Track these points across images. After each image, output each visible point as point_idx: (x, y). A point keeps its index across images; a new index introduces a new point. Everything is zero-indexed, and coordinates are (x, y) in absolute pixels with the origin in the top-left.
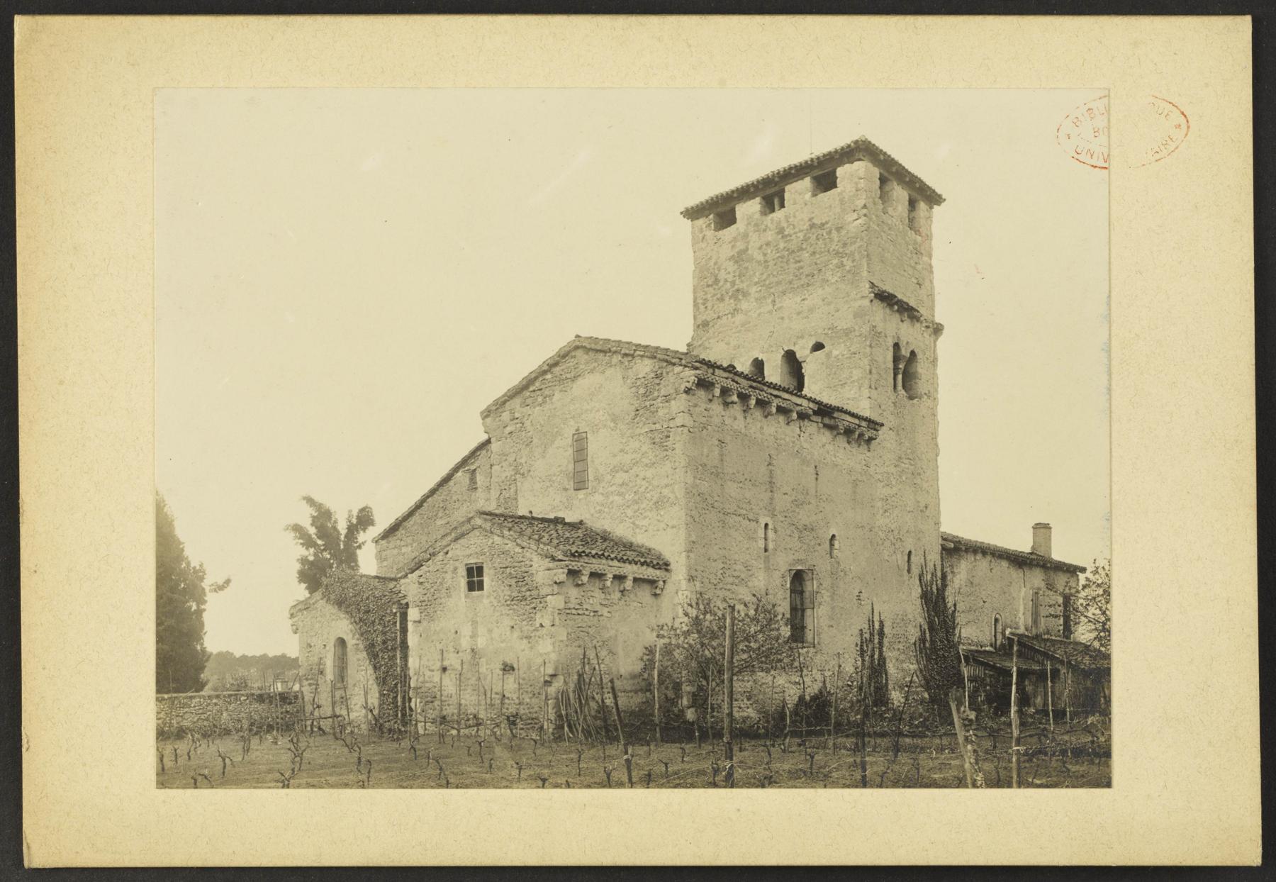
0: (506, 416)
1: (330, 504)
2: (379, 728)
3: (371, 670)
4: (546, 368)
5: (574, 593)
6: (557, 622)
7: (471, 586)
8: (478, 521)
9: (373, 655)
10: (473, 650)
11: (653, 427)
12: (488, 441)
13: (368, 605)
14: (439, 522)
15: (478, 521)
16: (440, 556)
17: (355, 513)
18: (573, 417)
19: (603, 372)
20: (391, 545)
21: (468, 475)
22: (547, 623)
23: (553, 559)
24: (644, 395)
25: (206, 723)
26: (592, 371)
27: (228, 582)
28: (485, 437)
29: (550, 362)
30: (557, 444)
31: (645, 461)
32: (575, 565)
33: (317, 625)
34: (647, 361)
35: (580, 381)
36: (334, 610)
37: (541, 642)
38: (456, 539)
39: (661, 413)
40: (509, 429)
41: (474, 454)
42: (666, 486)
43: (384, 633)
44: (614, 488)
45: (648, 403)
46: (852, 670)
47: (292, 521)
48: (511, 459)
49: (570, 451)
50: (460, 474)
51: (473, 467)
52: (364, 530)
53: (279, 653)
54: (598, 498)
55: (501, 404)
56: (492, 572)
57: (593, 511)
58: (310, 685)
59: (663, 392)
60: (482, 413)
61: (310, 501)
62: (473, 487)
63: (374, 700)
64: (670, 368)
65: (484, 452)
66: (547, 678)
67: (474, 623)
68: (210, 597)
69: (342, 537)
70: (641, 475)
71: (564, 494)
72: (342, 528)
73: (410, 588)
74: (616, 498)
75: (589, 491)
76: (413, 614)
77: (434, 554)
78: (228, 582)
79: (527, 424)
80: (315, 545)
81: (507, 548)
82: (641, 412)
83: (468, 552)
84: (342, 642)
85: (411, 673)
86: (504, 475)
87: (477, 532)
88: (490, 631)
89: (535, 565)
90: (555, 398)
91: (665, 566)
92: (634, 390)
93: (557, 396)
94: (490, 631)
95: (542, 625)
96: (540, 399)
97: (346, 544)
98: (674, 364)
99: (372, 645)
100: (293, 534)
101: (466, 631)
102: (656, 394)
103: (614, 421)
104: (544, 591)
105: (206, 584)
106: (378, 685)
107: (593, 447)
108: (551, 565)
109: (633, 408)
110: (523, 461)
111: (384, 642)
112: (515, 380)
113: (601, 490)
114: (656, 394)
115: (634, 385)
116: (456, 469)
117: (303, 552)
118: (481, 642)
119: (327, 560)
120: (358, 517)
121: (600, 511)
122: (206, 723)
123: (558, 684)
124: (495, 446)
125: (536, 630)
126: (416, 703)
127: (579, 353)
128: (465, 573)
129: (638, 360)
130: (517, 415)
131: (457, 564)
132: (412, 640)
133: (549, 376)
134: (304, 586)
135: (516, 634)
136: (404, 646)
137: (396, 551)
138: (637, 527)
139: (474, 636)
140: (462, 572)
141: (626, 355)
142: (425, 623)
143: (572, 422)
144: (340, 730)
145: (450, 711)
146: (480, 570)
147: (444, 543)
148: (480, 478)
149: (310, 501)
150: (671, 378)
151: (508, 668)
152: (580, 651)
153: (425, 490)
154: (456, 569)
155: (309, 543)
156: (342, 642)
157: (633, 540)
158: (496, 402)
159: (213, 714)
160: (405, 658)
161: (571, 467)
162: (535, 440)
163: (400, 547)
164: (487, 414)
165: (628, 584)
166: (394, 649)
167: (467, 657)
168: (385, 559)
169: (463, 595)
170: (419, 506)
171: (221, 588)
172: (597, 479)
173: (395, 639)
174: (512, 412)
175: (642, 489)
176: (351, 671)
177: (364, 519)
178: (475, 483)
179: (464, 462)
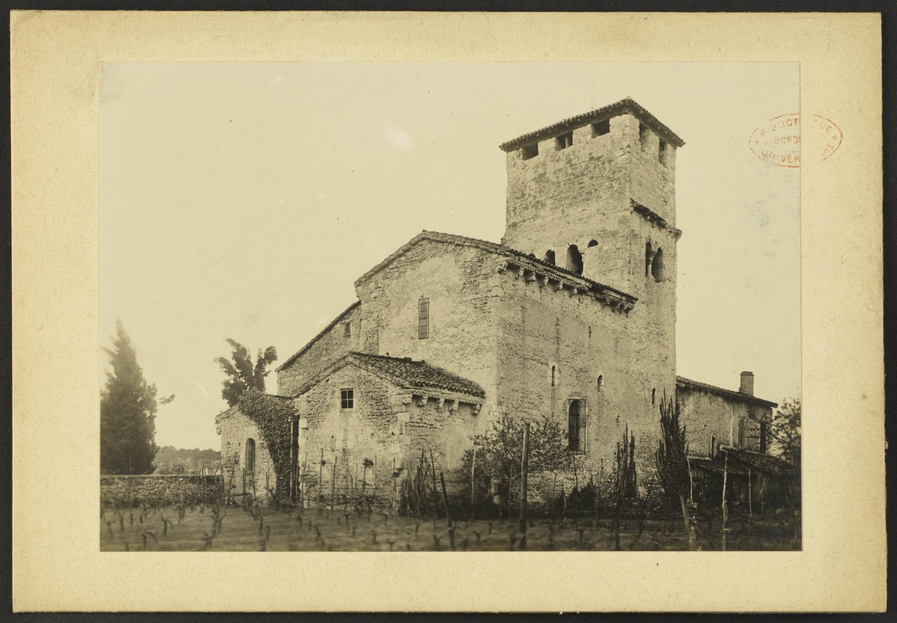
0: (372, 285)
3: (271, 462)
4: (401, 252)
8: (350, 359)
9: (272, 447)
12: (359, 303)
15: (350, 359)
16: (323, 383)
17: (263, 351)
18: (419, 288)
20: (288, 374)
23: (403, 387)
25: (154, 497)
27: (173, 397)
28: (357, 300)
29: (405, 248)
31: (470, 320)
32: (419, 392)
34: (473, 250)
35: (425, 263)
37: (392, 445)
38: (335, 371)
39: (481, 286)
40: (374, 295)
41: (348, 312)
42: (484, 338)
43: (282, 436)
44: (447, 338)
50: (338, 325)
51: (348, 321)
52: (270, 363)
54: (435, 345)
55: (368, 277)
56: (359, 395)
58: (228, 471)
59: (483, 272)
60: (355, 283)
61: (232, 342)
62: (347, 335)
63: (273, 483)
64: (488, 255)
66: (396, 471)
68: (160, 407)
69: (254, 368)
70: (466, 330)
71: (412, 341)
72: (254, 362)
73: (301, 405)
75: (429, 340)
76: (303, 423)
77: (318, 381)
78: (173, 397)
79: (387, 291)
80: (234, 373)
81: (370, 378)
84: (251, 442)
85: (300, 464)
87: (349, 367)
88: (356, 437)
89: (390, 391)
90: (407, 274)
91: (481, 394)
92: (463, 269)
93: (409, 272)
94: (356, 437)
95: (393, 434)
96: (397, 274)
97: (256, 372)
98: (492, 253)
100: (219, 364)
104: (395, 410)
105: (157, 398)
106: (276, 472)
107: (433, 309)
108: (401, 391)
109: (462, 282)
110: (383, 317)
111: (282, 442)
113: (438, 340)
115: (463, 266)
117: (226, 377)
118: (350, 445)
119: (243, 385)
122: (154, 497)
124: (363, 306)
125: (389, 437)
127: (425, 242)
128: (340, 395)
130: (380, 285)
131: (335, 388)
132: (301, 441)
133: (403, 258)
134: (226, 401)
135: (375, 439)
136: (296, 446)
137: (292, 379)
140: (338, 394)
141: (458, 245)
142: (311, 430)
143: (418, 291)
145: (326, 492)
146: (351, 393)
147: (326, 373)
148: (352, 328)
149: (232, 342)
150: (489, 262)
151: (368, 463)
152: (420, 452)
154: (334, 392)
155: (230, 370)
156: (251, 442)
157: (460, 375)
158: (365, 276)
161: (417, 322)
162: (392, 303)
164: (359, 283)
166: (288, 448)
167: (339, 454)
169: (338, 411)
170: (309, 347)
171: (168, 401)
172: (435, 331)
173: (289, 441)
174: (376, 283)
175: (467, 340)
176: (258, 461)
177: (270, 356)
178: (349, 332)
179: (342, 317)
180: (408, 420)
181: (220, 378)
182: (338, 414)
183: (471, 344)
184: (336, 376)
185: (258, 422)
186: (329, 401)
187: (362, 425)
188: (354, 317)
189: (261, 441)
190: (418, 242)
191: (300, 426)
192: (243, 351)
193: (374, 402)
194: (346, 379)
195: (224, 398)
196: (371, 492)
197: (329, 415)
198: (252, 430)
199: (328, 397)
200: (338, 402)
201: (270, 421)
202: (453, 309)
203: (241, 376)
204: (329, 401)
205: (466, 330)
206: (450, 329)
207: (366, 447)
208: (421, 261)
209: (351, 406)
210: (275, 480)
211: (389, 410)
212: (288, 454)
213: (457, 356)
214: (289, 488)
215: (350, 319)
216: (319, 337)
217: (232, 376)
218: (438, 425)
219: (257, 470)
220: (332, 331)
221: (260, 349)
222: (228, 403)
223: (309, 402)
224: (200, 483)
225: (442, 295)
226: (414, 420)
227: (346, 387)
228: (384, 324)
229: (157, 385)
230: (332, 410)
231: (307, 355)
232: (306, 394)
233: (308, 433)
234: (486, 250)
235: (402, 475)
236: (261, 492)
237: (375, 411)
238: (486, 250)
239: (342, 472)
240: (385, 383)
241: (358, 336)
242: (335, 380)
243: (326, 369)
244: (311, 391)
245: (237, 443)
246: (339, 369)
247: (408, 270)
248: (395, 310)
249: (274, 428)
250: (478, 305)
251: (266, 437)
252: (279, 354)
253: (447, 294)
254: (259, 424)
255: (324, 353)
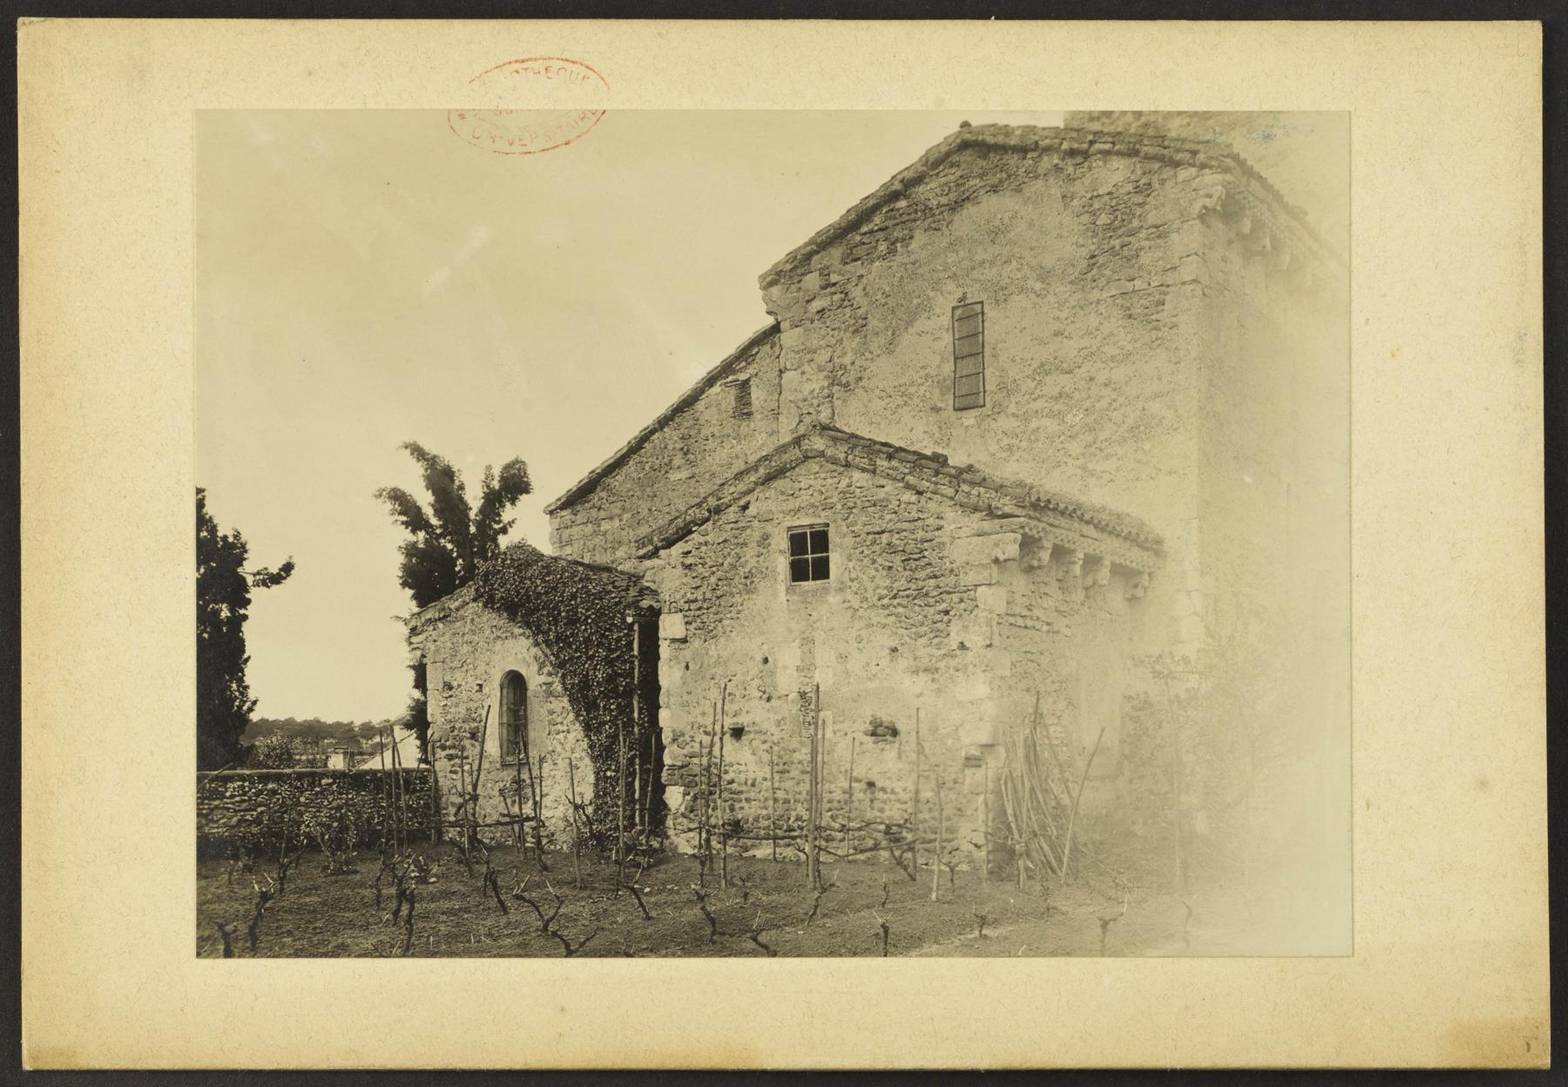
0: (812, 281)
1: (449, 456)
2: (594, 840)
3: (577, 731)
4: (897, 186)
5: (1020, 583)
6: (996, 642)
7: (799, 572)
8: (819, 443)
9: (583, 699)
10: (803, 695)
11: (1129, 286)
12: (776, 329)
13: (574, 610)
14: (674, 476)
15: (819, 443)
16: (731, 514)
17: (497, 472)
18: (954, 277)
19: (1018, 190)
20: (580, 518)
21: (732, 393)
22: (975, 640)
23: (991, 513)
24: (1108, 227)
25: (255, 830)
26: (995, 189)
27: (288, 568)
28: (769, 321)
29: (909, 175)
30: (919, 325)
31: (1111, 350)
32: (1035, 528)
33: (466, 648)
34: (1117, 163)
35: (970, 210)
36: (500, 620)
37: (960, 677)
38: (769, 479)
39: (1146, 259)
40: (817, 305)
41: (746, 353)
42: (1156, 396)
43: (610, 663)
44: (1040, 404)
45: (1116, 243)
46: (1089, 739)
47: (390, 483)
48: (822, 357)
49: (947, 338)
50: (716, 389)
51: (743, 377)
52: (513, 501)
53: (310, 717)
54: (1005, 422)
55: (801, 261)
56: (849, 541)
57: (993, 448)
58: (450, 758)
59: (1152, 218)
60: (762, 277)
61: (418, 452)
62: (743, 410)
63: (587, 791)
64: (1168, 172)
65: (767, 348)
66: (975, 752)
67: (807, 642)
68: (256, 594)
69: (472, 515)
70: (1102, 377)
71: (933, 417)
72: (474, 498)
73: (668, 577)
74: (1046, 422)
75: (987, 410)
76: (671, 626)
77: (718, 510)
78: (288, 568)
79: (856, 293)
80: (426, 526)
81: (882, 494)
82: (1101, 260)
83: (792, 504)
84: (515, 681)
85: (666, 738)
86: (807, 388)
87: (814, 466)
88: (843, 658)
89: (949, 528)
90: (914, 245)
91: (1155, 547)
92: (1086, 218)
93: (920, 238)
94: (843, 658)
95: (962, 646)
96: (883, 247)
97: (479, 525)
98: (1177, 164)
99: (585, 685)
100: (389, 505)
101: (788, 657)
102: (1136, 223)
103: (1042, 279)
104: (968, 579)
105: (248, 568)
106: (594, 759)
107: (997, 325)
108: (987, 525)
109: (1085, 252)
110: (847, 361)
111: (610, 679)
112: (832, 213)
113: (1012, 409)
114: (1136, 223)
115: (1088, 209)
116: (710, 381)
117: (405, 536)
118: (823, 677)
119: (452, 555)
120: (502, 478)
121: (1010, 448)
122: (255, 830)
123: (994, 764)
124: (789, 337)
125: (951, 655)
126: (675, 797)
127: (967, 157)
128: (785, 544)
129: (1097, 162)
130: (834, 278)
131: (769, 528)
132: (669, 675)
133: (903, 204)
134: (409, 592)
135: (903, 663)
136: (651, 688)
137: (589, 528)
138: (1092, 474)
139: (806, 668)
140: (781, 542)
141: (1072, 153)
142: (696, 644)
143: (951, 286)
144: (526, 843)
145: (747, 811)
146: (821, 540)
147: (742, 487)
148: (757, 395)
149: (418, 452)
150: (1171, 191)
151: (884, 732)
152: (1030, 699)
153: (648, 419)
154: (766, 537)
155: (415, 520)
156: (515, 681)
157: (1083, 499)
158: (792, 257)
159: (303, 840)
160: (653, 707)
161: (948, 368)
162: (873, 323)
163: (597, 522)
164: (773, 279)
165: (1104, 574)
166: (628, 694)
167: (791, 708)
168: (570, 543)
169: (782, 588)
170: (636, 448)
171: (276, 579)
172: (1002, 387)
173: (630, 674)
174: (825, 273)
175: (1104, 403)
176: (537, 732)
177: (513, 485)
178: (749, 404)
179: (727, 368)
180: (1002, 609)
181: (391, 542)
182: (783, 597)
183: (1117, 415)
184: (771, 493)
185: (534, 627)
186: (752, 563)
187: (858, 624)
188: (761, 369)
189: (543, 679)
190: (948, 154)
191: (662, 634)
192: (448, 473)
193: (898, 559)
194: (804, 498)
195: (405, 584)
196: (894, 813)
197: (758, 601)
198: (517, 651)
199: (750, 553)
200: (782, 564)
201: (573, 621)
202: (1057, 326)
203: (442, 535)
204: (752, 563)
205: (1102, 377)
206: (1049, 379)
207: (873, 685)
208: (955, 206)
209: (822, 571)
210: (592, 778)
211: (950, 580)
212: (626, 710)
213: (1075, 448)
214: (633, 801)
215: (751, 370)
216: (663, 422)
217: (421, 535)
218: (1060, 624)
219: (534, 753)
220: (700, 405)
221: (489, 468)
222: (415, 597)
223: (689, 567)
224: (378, 789)
225: (1022, 290)
226: (1017, 610)
227: (805, 521)
228: (850, 377)
229: (244, 538)
230: (762, 586)
231: (631, 467)
232: (678, 548)
233: (687, 653)
234: (1160, 158)
235: (992, 763)
236: (555, 812)
237: (901, 584)
238: (1160, 158)
239: (797, 756)
240: (931, 505)
241: (776, 414)
242: (771, 505)
243: (739, 476)
244: (695, 538)
245: (472, 683)
246: (781, 473)
247: (917, 234)
248: (882, 340)
249: (587, 641)
250: (1137, 311)
251: (561, 665)
252: (534, 476)
253: (1038, 286)
254: (539, 631)
255: (677, 461)
